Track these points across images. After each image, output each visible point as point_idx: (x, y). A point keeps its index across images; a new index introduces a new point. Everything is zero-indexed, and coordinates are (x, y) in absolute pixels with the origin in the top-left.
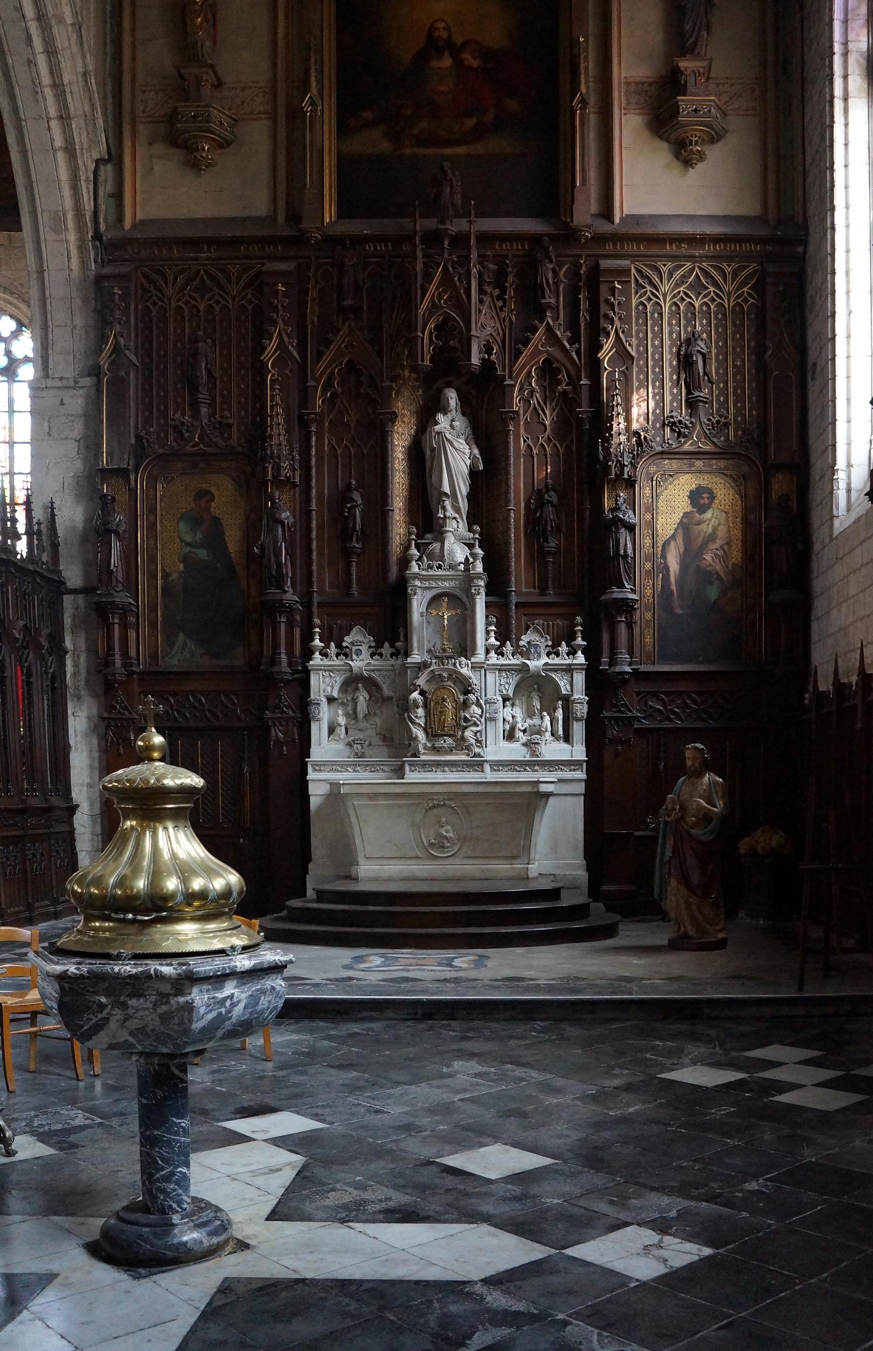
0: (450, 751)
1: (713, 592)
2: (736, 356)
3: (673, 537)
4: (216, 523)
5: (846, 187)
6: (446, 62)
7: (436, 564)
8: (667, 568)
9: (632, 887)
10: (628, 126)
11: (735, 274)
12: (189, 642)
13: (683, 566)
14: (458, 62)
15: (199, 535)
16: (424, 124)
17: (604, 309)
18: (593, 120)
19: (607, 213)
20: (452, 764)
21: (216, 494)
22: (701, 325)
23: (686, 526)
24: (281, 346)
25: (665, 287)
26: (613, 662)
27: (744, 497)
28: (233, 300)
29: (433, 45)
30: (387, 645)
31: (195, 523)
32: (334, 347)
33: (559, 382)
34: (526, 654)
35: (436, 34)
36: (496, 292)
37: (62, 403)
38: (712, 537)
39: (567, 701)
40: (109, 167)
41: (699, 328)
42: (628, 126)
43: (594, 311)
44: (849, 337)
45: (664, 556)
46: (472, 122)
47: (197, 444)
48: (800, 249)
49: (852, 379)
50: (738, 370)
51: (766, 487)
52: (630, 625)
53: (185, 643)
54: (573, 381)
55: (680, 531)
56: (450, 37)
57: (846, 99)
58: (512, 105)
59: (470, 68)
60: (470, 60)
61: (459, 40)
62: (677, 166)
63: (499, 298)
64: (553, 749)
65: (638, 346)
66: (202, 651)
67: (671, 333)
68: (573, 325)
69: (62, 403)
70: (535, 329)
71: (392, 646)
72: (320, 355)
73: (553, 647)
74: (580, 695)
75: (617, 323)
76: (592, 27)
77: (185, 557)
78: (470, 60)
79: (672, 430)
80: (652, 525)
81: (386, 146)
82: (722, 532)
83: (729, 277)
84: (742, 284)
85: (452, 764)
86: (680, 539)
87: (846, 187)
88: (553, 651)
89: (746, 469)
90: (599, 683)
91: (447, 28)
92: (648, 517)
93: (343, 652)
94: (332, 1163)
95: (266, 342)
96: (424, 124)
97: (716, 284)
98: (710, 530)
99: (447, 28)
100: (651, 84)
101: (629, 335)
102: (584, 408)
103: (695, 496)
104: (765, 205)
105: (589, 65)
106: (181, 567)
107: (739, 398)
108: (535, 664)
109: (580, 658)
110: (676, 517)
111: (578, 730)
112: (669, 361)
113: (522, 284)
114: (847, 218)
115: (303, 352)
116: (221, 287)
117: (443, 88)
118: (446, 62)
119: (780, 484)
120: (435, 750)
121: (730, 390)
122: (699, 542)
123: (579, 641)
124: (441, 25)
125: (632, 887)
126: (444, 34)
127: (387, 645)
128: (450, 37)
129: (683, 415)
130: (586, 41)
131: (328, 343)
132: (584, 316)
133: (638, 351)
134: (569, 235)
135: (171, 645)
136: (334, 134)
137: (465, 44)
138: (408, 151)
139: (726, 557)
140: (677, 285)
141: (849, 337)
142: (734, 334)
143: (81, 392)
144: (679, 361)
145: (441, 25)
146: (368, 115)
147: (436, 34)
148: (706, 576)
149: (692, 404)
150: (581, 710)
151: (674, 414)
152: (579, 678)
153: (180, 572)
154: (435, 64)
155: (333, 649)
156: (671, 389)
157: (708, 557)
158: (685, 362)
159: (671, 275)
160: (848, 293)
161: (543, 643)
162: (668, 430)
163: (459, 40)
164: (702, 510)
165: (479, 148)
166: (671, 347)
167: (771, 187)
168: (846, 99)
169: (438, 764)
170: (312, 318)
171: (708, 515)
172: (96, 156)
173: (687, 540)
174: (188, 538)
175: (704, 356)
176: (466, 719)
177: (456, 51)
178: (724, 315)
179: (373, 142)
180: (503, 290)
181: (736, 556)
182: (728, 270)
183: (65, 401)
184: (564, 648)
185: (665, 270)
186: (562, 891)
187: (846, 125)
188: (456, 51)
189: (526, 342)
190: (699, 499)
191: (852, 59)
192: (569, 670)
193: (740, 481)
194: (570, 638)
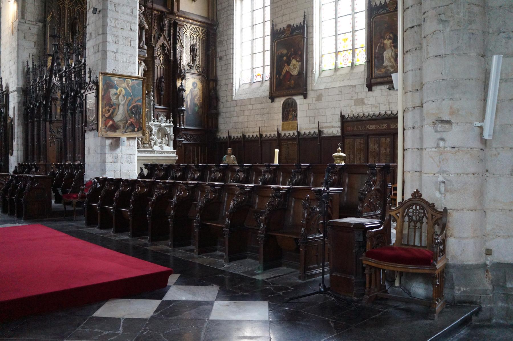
0: (148, 148)
1: (197, 109)
13: (191, 102)
20: (148, 152)
23: (191, 92)
24: (52, 17)
25: (188, 31)
26: (180, 126)
27: (203, 86)
34: (160, 122)
37: (30, 29)
38: (196, 95)
39: (168, 135)
48: (215, 28)
51: (208, 84)
52: (183, 116)
54: (169, 51)
64: (166, 148)
69: (30, 29)
70: (161, 36)
74: (172, 134)
82: (198, 94)
85: (148, 152)
88: (166, 122)
89: (203, 79)
90: (177, 131)
94: (422, 83)
103: (193, 84)
104: (208, 15)
107: (202, 61)
108: (163, 125)
109: (172, 124)
111: (172, 143)
120: (144, 147)
123: (171, 119)
134: (172, 12)
139: (199, 100)
143: (37, 27)
148: (195, 105)
149: (193, 61)
150: (172, 137)
152: (172, 129)
157: (196, 100)
161: (164, 119)
164: (195, 88)
167: (498, 88)
169: (145, 152)
171: (196, 89)
176: (151, 139)
181: (201, 101)
183: (31, 28)
184: (168, 121)
186: (342, 114)
189: (159, 38)
192: (170, 127)
193: (202, 81)
194: (169, 119)
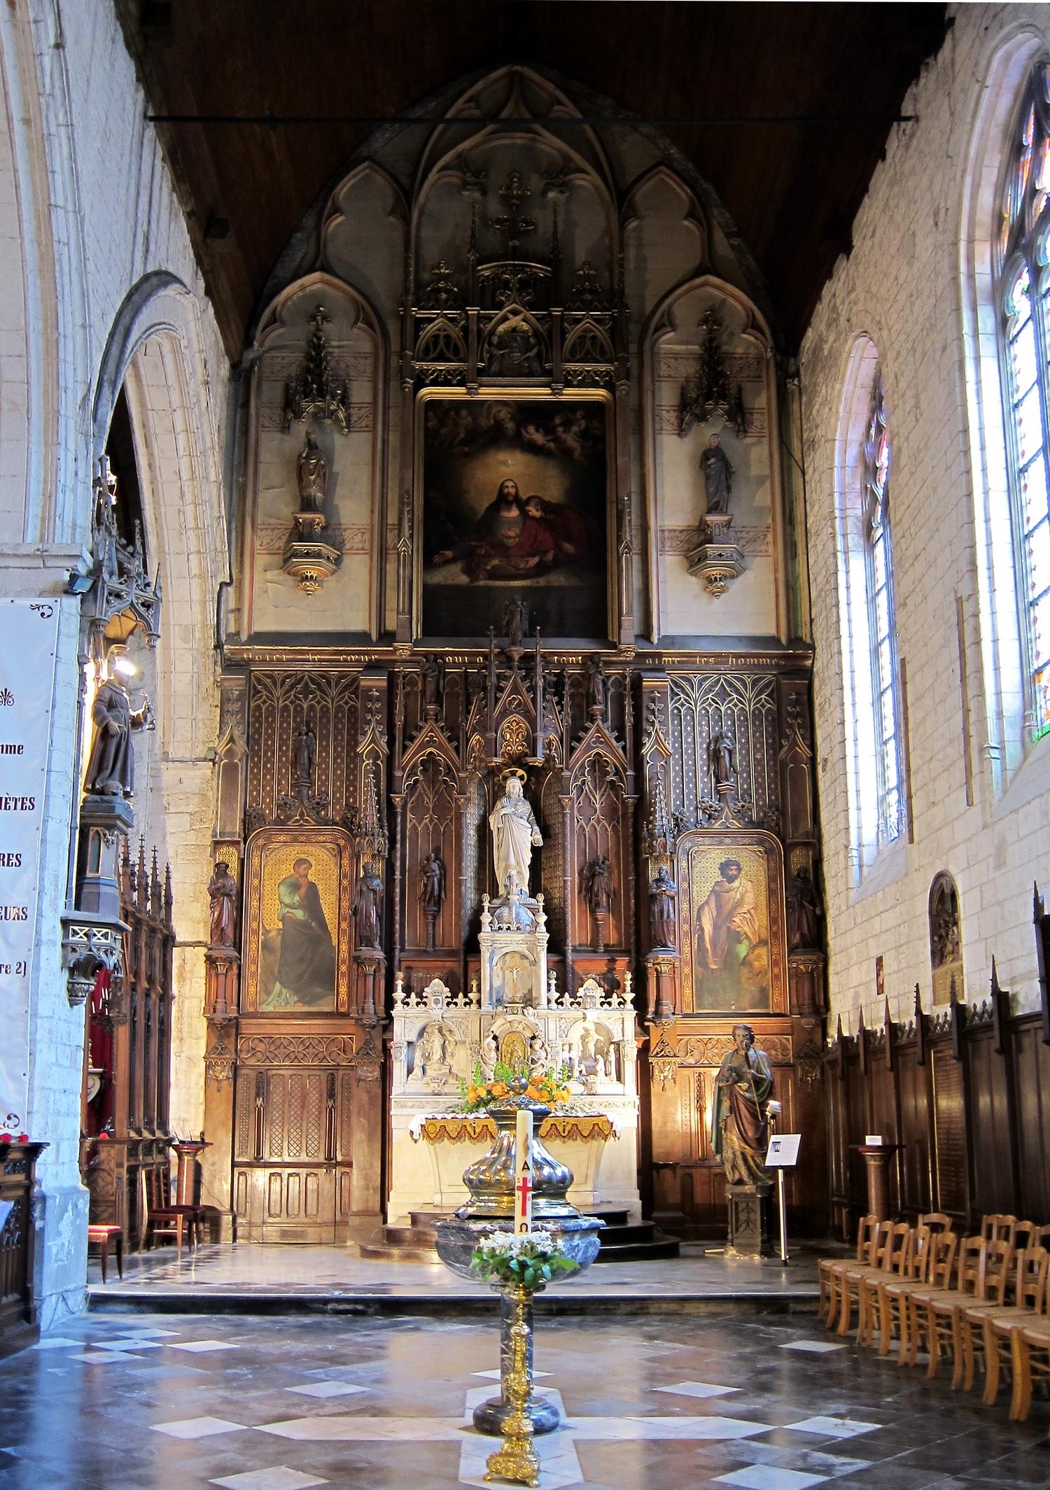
2: (756, 750)
3: (707, 902)
4: (312, 887)
5: (849, 621)
6: (514, 513)
7: (505, 926)
8: (702, 929)
9: (680, 1214)
10: (668, 569)
11: (755, 683)
12: (284, 991)
13: (716, 927)
14: (524, 514)
15: (297, 898)
16: (496, 562)
17: (645, 713)
18: (636, 559)
19: (646, 635)
21: (313, 863)
22: (727, 725)
23: (717, 893)
28: (333, 700)
29: (504, 499)
30: (461, 995)
31: (295, 887)
32: (417, 742)
33: (607, 773)
35: (506, 491)
36: (556, 699)
38: (740, 903)
40: (231, 589)
41: (725, 728)
42: (668, 569)
43: (638, 709)
44: (856, 740)
45: (699, 919)
46: (536, 559)
47: (297, 821)
49: (861, 775)
50: (758, 762)
53: (281, 992)
55: (713, 898)
56: (517, 493)
57: (846, 553)
58: (568, 547)
59: (534, 518)
60: (534, 512)
61: (524, 496)
62: (705, 597)
63: (558, 703)
65: (673, 743)
66: (296, 998)
67: (701, 733)
68: (619, 728)
70: (586, 730)
71: (465, 996)
72: (405, 748)
73: (606, 997)
75: (657, 725)
76: (634, 486)
77: (284, 916)
78: (534, 512)
79: (704, 812)
80: (689, 892)
81: (464, 579)
83: (749, 686)
84: (760, 693)
86: (713, 904)
87: (849, 621)
91: (516, 487)
92: (685, 885)
93: (422, 1001)
95: (360, 738)
96: (496, 562)
97: (738, 692)
98: (738, 896)
99: (516, 487)
100: (681, 531)
101: (666, 734)
102: (629, 797)
103: (724, 867)
105: (633, 518)
106: (280, 925)
110: (709, 886)
112: (701, 755)
113: (576, 695)
114: (851, 645)
115: (391, 743)
116: (322, 691)
117: (512, 534)
118: (514, 513)
119: (799, 859)
121: (753, 780)
122: (729, 906)
124: (510, 484)
125: (680, 1214)
126: (512, 491)
127: (461, 995)
128: (517, 493)
129: (714, 803)
130: (630, 499)
131: (412, 739)
132: (629, 721)
133: (673, 747)
135: (268, 993)
136: (421, 568)
137: (529, 499)
138: (482, 583)
140: (706, 693)
141: (856, 740)
142: (754, 732)
144: (709, 755)
145: (510, 484)
146: (449, 554)
147: (506, 491)
151: (706, 799)
153: (279, 930)
154: (505, 514)
155: (413, 999)
156: (702, 778)
158: (715, 756)
159: (700, 684)
160: (854, 705)
162: (700, 812)
163: (524, 496)
164: (731, 880)
165: (542, 582)
166: (701, 744)
168: (846, 553)
170: (399, 722)
171: (736, 884)
172: (220, 580)
173: (719, 906)
174: (287, 900)
175: (730, 752)
177: (522, 505)
178: (746, 719)
179: (454, 575)
180: (561, 697)
182: (748, 681)
185: (695, 681)
187: (847, 572)
188: (522, 505)
190: (728, 870)
191: (850, 522)
